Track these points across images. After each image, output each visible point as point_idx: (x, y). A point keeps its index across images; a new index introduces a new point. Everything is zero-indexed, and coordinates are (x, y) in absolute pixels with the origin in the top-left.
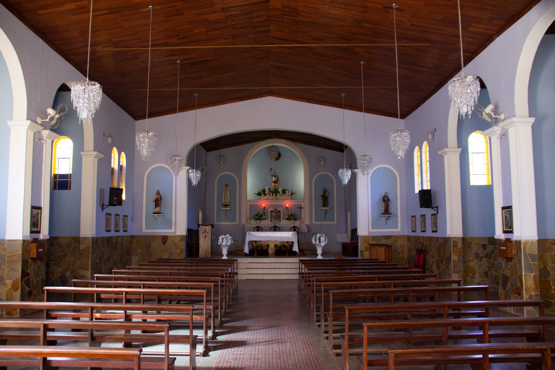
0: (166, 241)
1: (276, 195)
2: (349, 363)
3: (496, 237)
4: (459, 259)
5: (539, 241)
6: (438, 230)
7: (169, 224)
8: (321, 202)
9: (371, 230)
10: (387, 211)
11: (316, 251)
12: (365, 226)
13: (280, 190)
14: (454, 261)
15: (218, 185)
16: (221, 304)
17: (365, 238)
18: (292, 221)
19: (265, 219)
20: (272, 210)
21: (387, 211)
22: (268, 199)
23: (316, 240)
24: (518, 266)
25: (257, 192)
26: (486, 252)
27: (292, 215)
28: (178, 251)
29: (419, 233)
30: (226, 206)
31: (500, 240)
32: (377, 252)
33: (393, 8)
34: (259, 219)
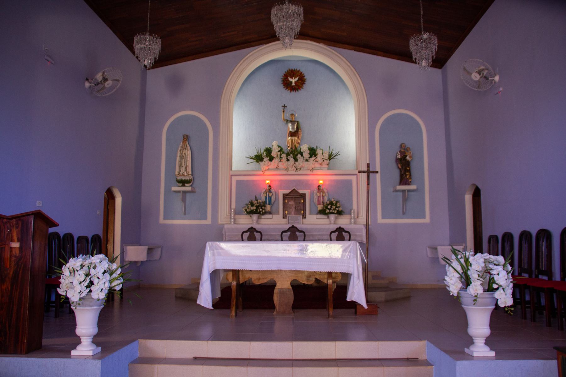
1: (296, 160)
8: (396, 174)
11: (463, 321)
13: (304, 148)
15: (167, 139)
18: (332, 217)
19: (270, 213)
20: (287, 192)
22: (277, 168)
23: (466, 281)
25: (254, 153)
27: (331, 203)
30: (183, 183)
34: (256, 212)
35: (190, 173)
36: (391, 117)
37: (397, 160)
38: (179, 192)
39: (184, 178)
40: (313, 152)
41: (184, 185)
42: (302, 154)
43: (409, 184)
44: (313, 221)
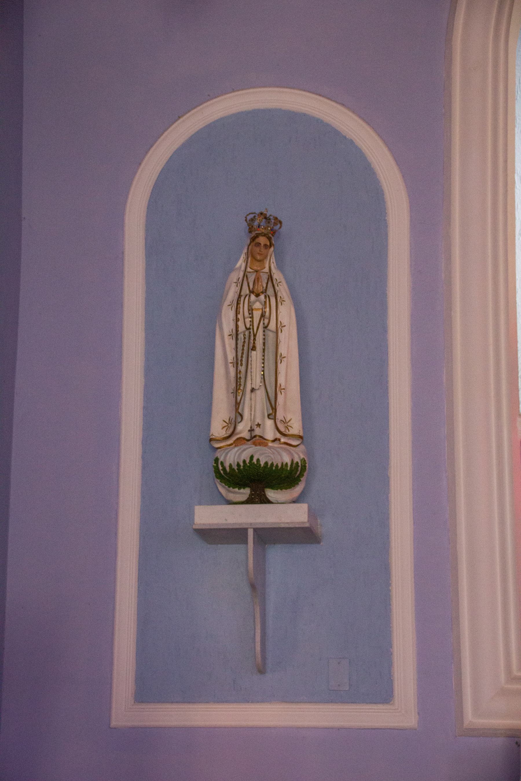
15: (153, 249)
30: (257, 481)
35: (296, 428)
38: (235, 535)
39: (264, 456)
41: (258, 498)
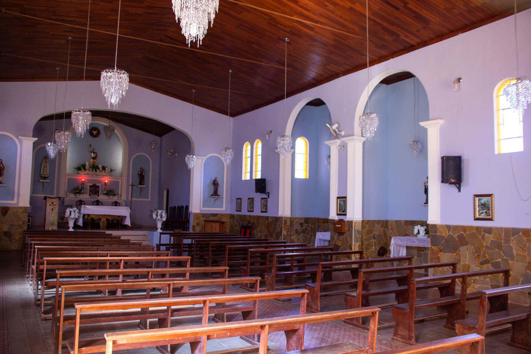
0: (7, 212)
1: (96, 171)
2: (320, 302)
3: (330, 218)
4: (287, 234)
5: (363, 221)
6: (268, 211)
7: (11, 195)
8: (138, 180)
9: (202, 209)
10: (216, 193)
12: (197, 204)
13: (100, 166)
14: (284, 235)
16: (257, 262)
17: (197, 215)
18: (111, 196)
20: (91, 184)
21: (216, 193)
22: (88, 174)
23: (157, 215)
24: (349, 238)
25: (77, 167)
26: (303, 228)
27: (111, 191)
28: (21, 223)
29: (244, 212)
30: (45, 178)
31: (333, 220)
32: (211, 227)
33: (285, 41)
36: (138, 156)
37: (139, 174)
40: (104, 168)
41: (45, 179)
42: (99, 169)
43: (143, 185)
44: (102, 197)
